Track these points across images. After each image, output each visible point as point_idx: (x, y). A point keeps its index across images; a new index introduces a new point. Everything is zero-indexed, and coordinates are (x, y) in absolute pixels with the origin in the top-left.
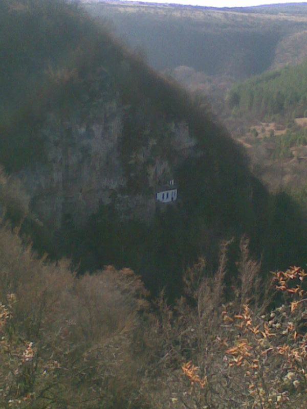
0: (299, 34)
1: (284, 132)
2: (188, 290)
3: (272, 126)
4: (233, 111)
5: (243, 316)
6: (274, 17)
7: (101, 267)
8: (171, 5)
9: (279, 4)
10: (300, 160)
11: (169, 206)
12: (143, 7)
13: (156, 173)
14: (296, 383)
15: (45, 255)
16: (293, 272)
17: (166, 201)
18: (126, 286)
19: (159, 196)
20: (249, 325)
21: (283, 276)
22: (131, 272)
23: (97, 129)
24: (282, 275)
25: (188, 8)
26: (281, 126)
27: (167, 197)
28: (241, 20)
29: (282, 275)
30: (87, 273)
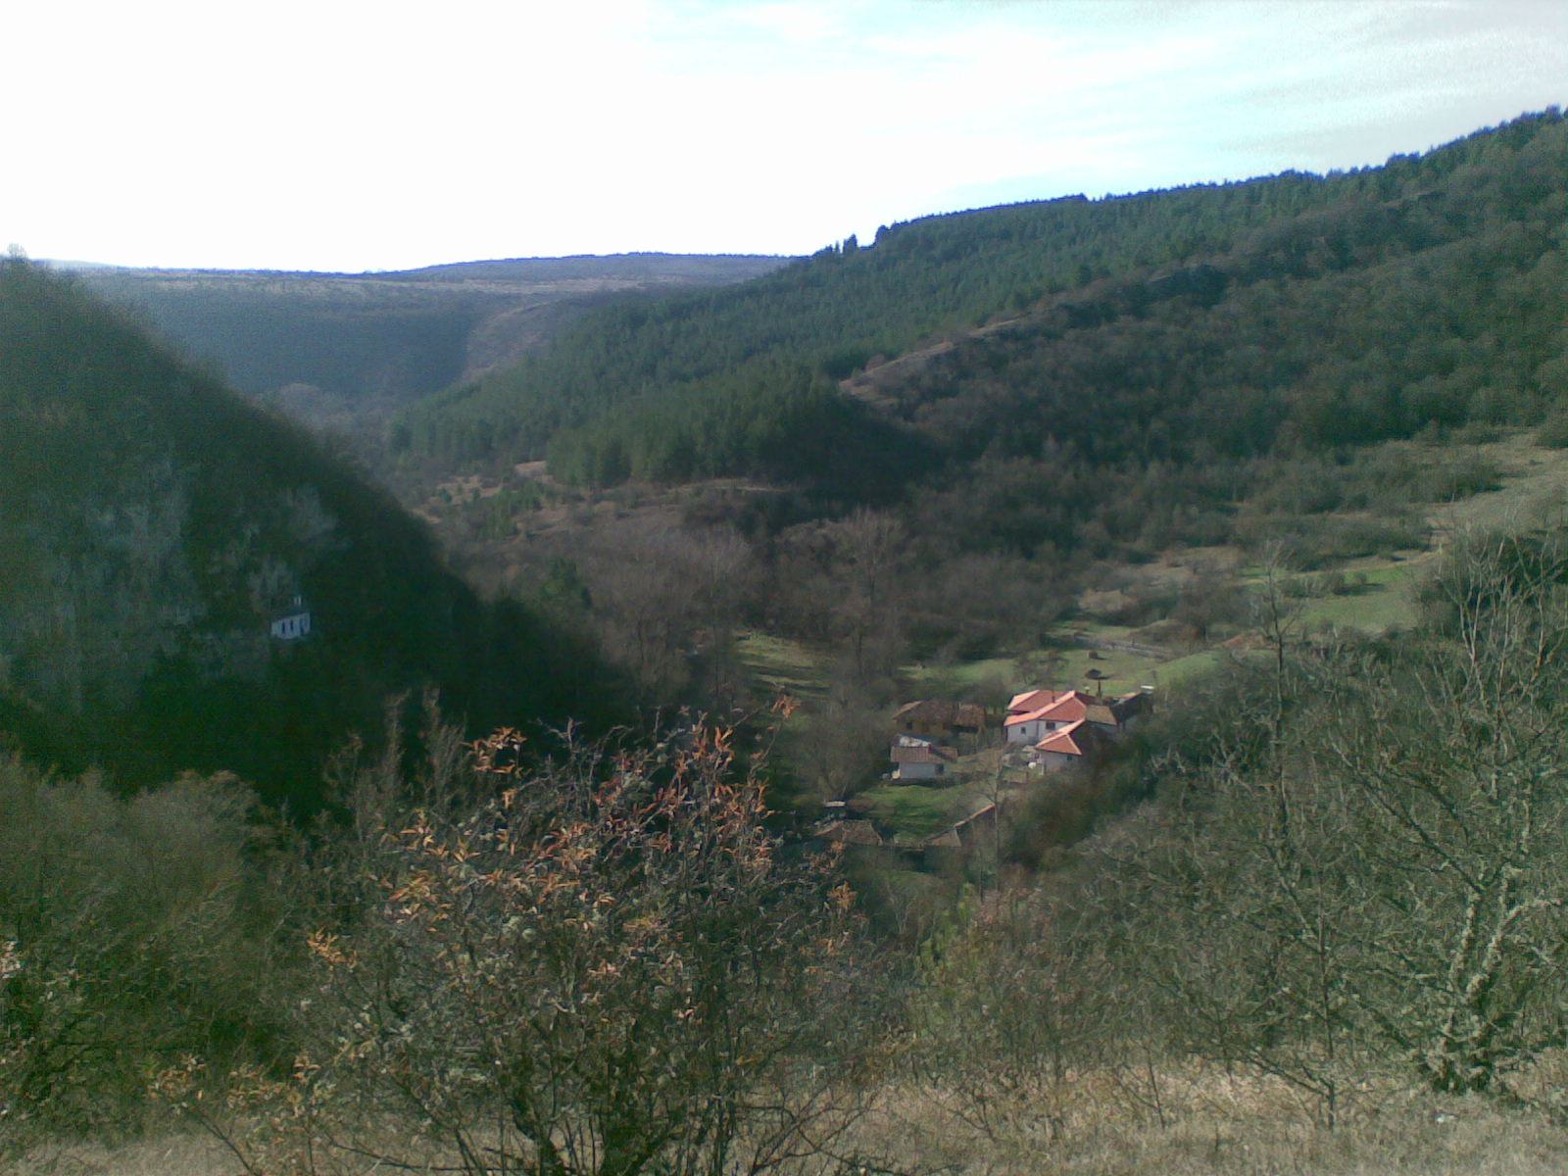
0: (505, 315)
1: (497, 490)
2: (335, 796)
3: (475, 482)
4: (401, 461)
5: (416, 830)
6: (455, 287)
7: (171, 776)
8: (261, 272)
9: (416, 270)
10: (530, 537)
11: (297, 645)
12: (208, 279)
13: (264, 585)
14: (528, 935)
15: (54, 768)
16: (502, 737)
17: (290, 635)
18: (225, 805)
19: (276, 629)
20: (429, 844)
21: (485, 748)
22: (233, 777)
23: (138, 514)
24: (481, 745)
25: (294, 277)
26: (491, 480)
27: (292, 627)
28: (397, 294)
29: (481, 745)
30: (144, 791)
